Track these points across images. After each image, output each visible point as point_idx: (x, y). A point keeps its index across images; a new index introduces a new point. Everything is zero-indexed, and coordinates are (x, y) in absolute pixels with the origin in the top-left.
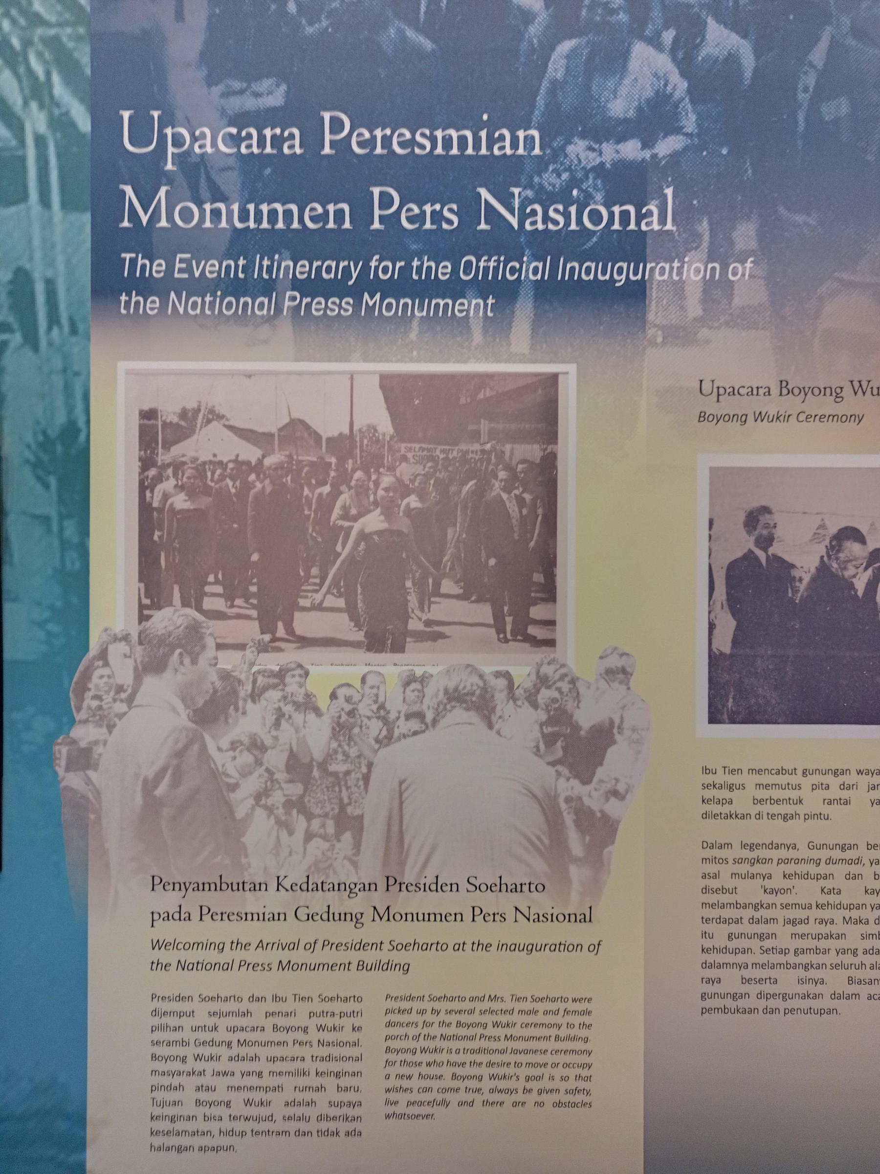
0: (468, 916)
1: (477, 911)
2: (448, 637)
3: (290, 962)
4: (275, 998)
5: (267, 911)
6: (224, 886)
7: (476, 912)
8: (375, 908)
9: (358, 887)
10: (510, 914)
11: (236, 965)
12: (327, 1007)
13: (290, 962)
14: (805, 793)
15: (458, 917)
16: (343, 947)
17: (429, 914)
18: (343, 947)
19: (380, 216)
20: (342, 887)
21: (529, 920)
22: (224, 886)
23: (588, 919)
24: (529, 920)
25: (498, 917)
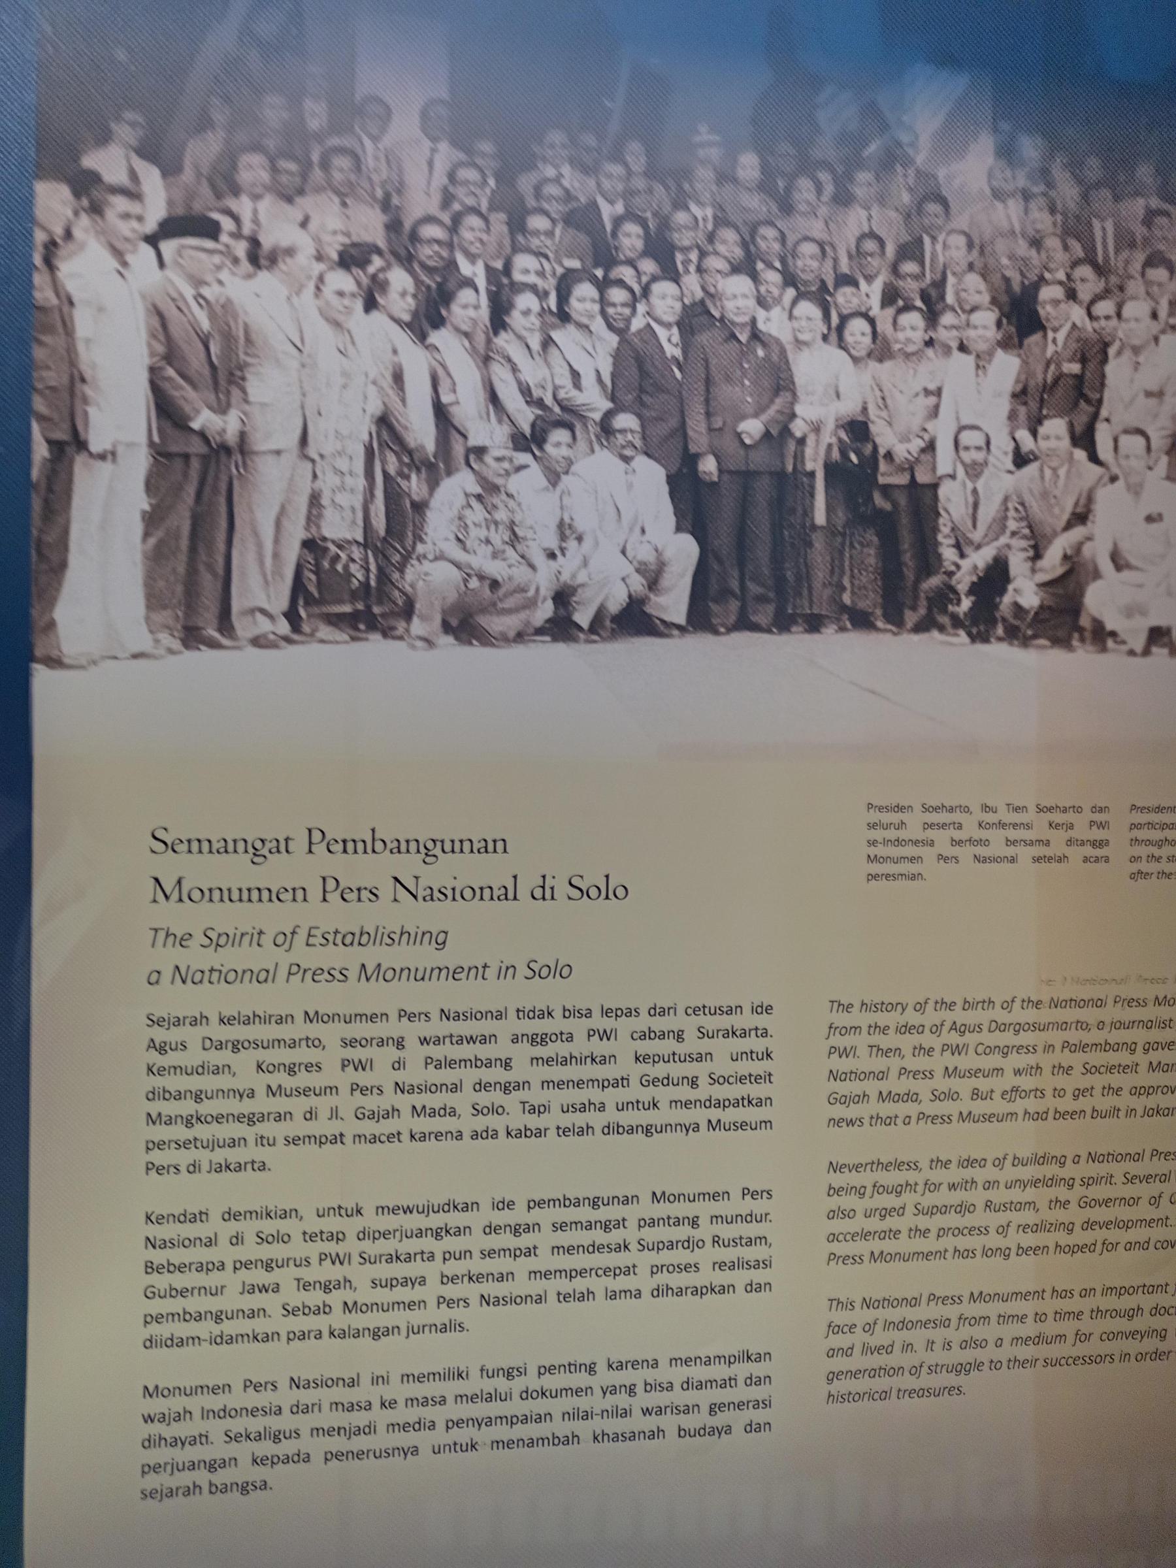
0: (315, 893)
1: (331, 884)
2: (1115, 545)
3: (379, 965)
4: (654, 1011)
6: (379, 846)
7: (331, 887)
8: (157, 880)
9: (268, 845)
10: (386, 889)
11: (282, 973)
13: (379, 965)
15: (299, 894)
17: (495, 841)
20: (413, 845)
21: (415, 897)
22: (379, 846)
23: (511, 895)
25: (365, 894)
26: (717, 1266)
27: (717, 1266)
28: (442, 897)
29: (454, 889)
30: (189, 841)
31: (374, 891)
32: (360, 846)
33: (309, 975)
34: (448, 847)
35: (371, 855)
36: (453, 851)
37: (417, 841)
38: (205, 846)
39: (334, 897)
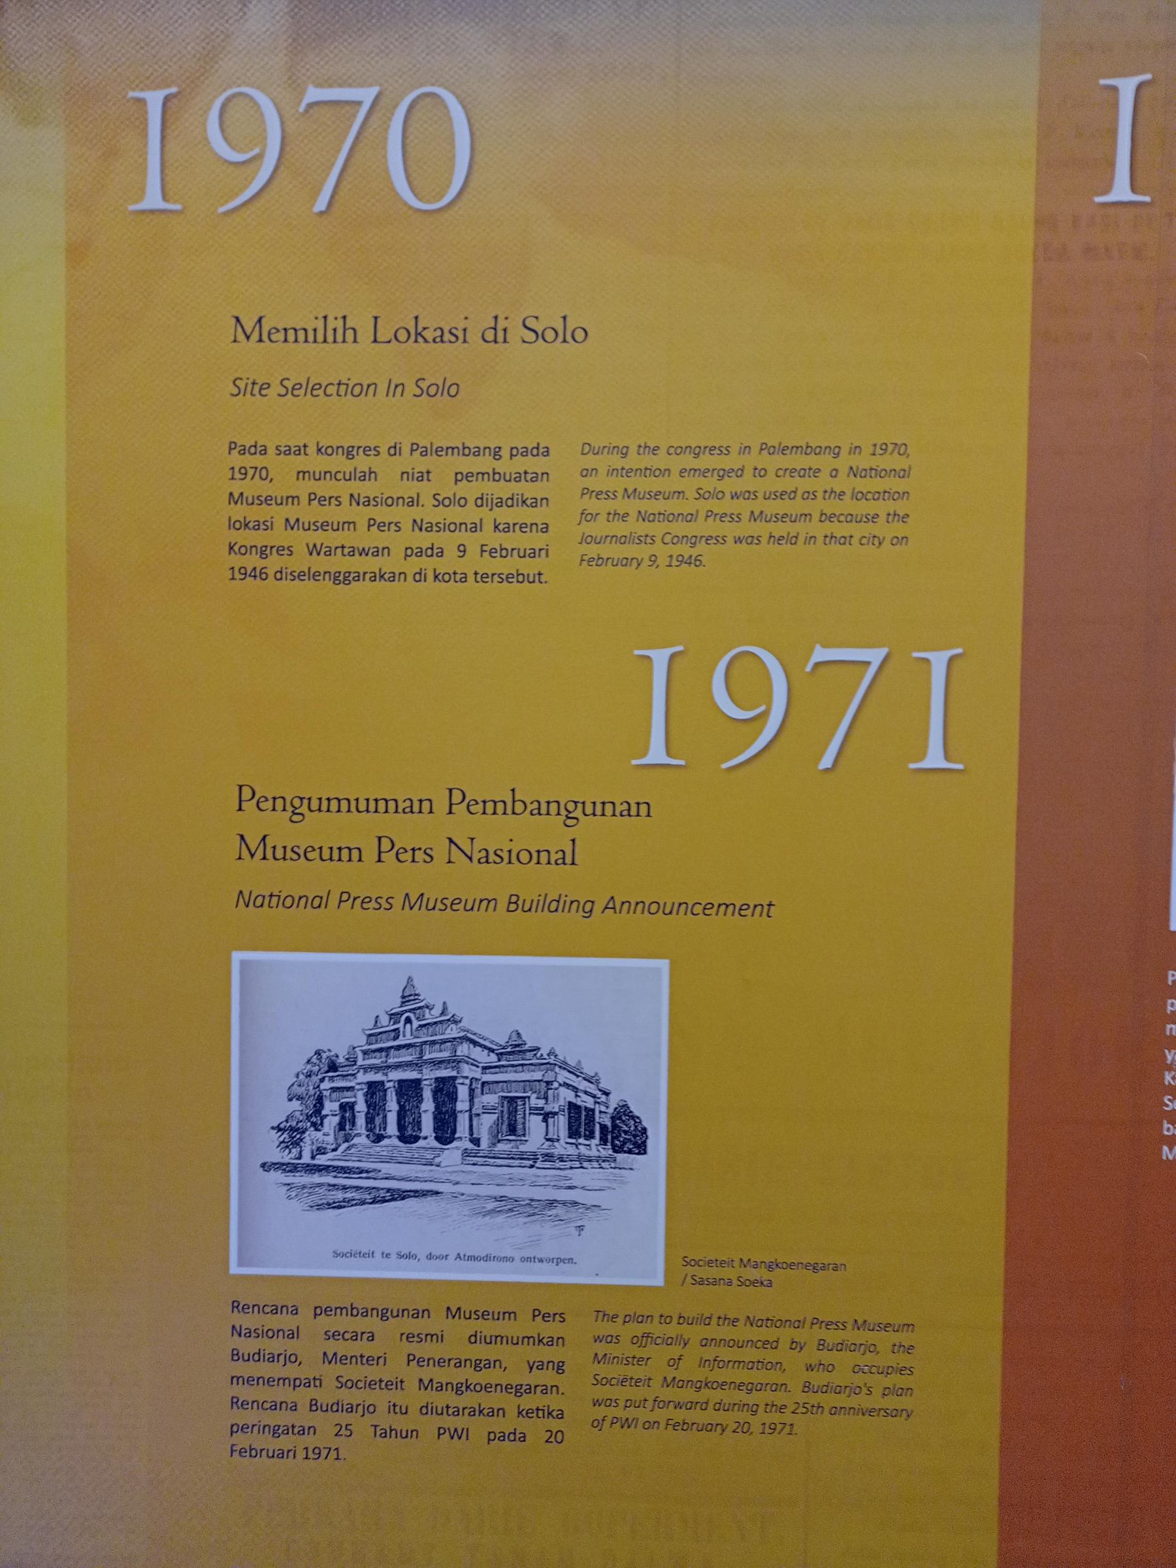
0: (370, 854)
5: (416, 471)
6: (519, 807)
12: (630, 551)
14: (398, 1352)
16: (373, 904)
18: (373, 904)
19: (417, 1083)
21: (470, 859)
22: (519, 807)
23: (568, 860)
24: (470, 859)
25: (419, 855)
26: (404, 1337)
27: (404, 1337)
28: (498, 860)
29: (510, 851)
30: (274, 798)
31: (428, 851)
32: (500, 806)
33: (358, 902)
34: (589, 810)
35: (511, 817)
36: (367, 811)
37: (283, 798)
38: (392, 805)
39: (390, 857)
